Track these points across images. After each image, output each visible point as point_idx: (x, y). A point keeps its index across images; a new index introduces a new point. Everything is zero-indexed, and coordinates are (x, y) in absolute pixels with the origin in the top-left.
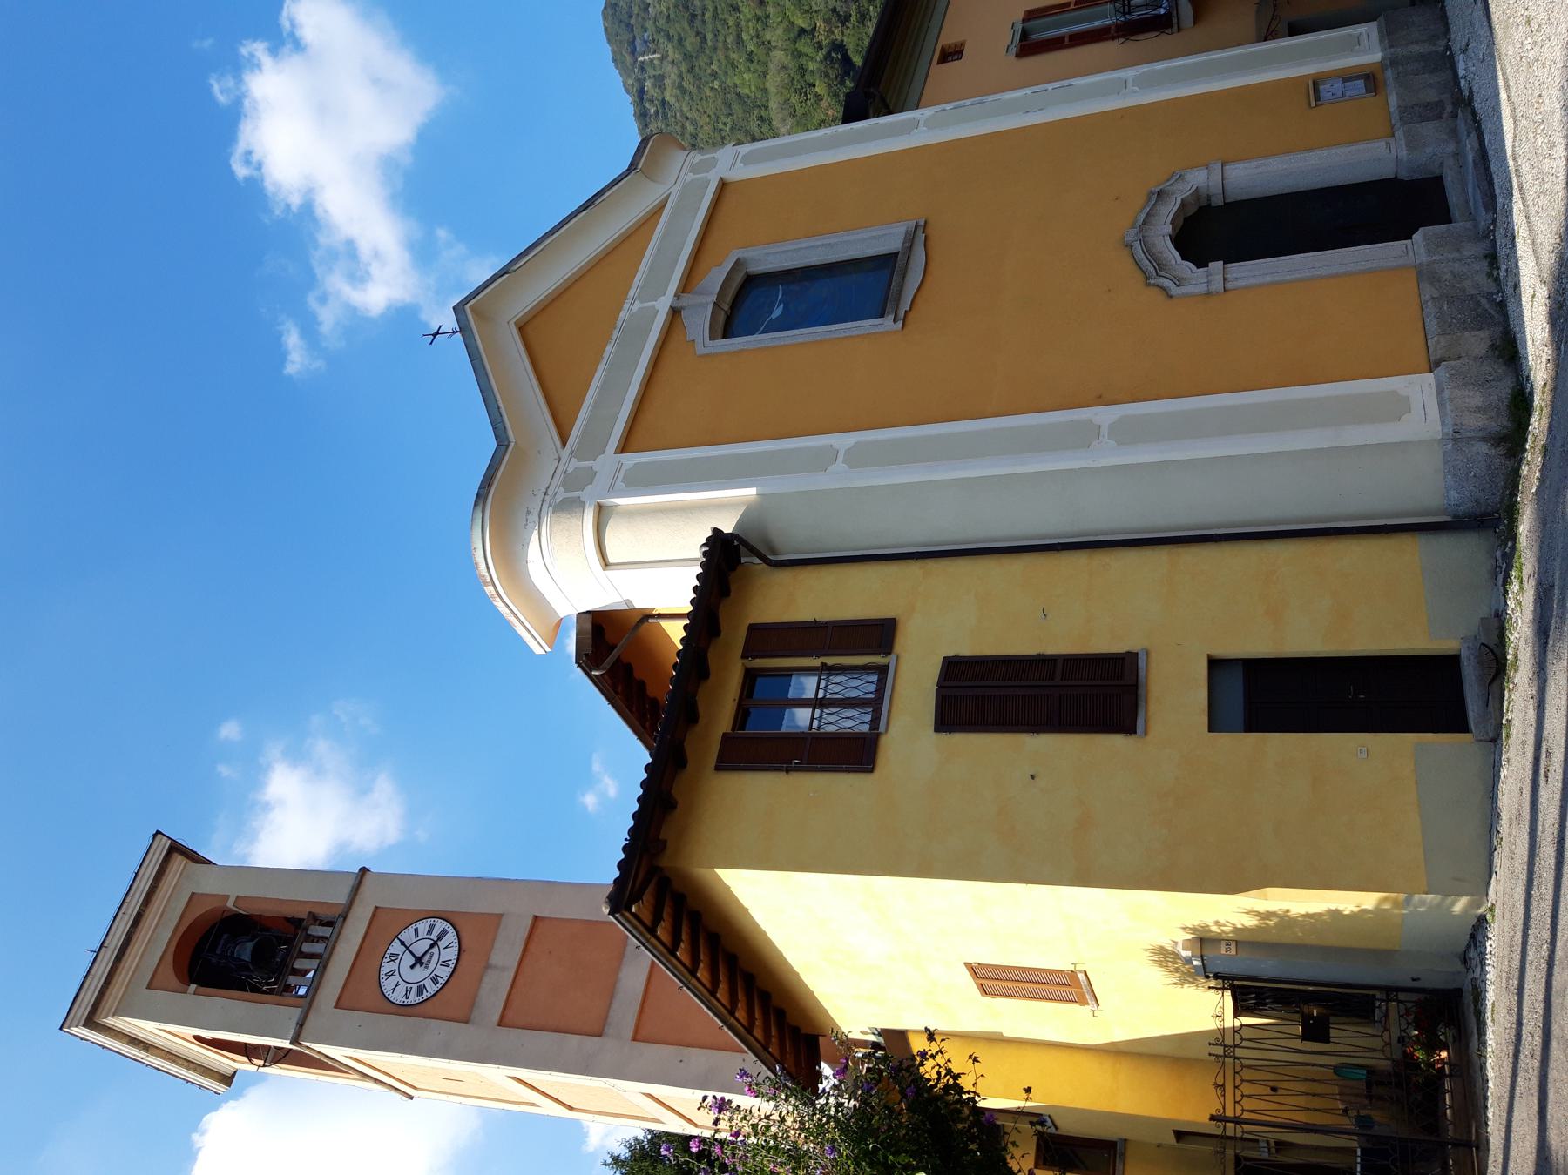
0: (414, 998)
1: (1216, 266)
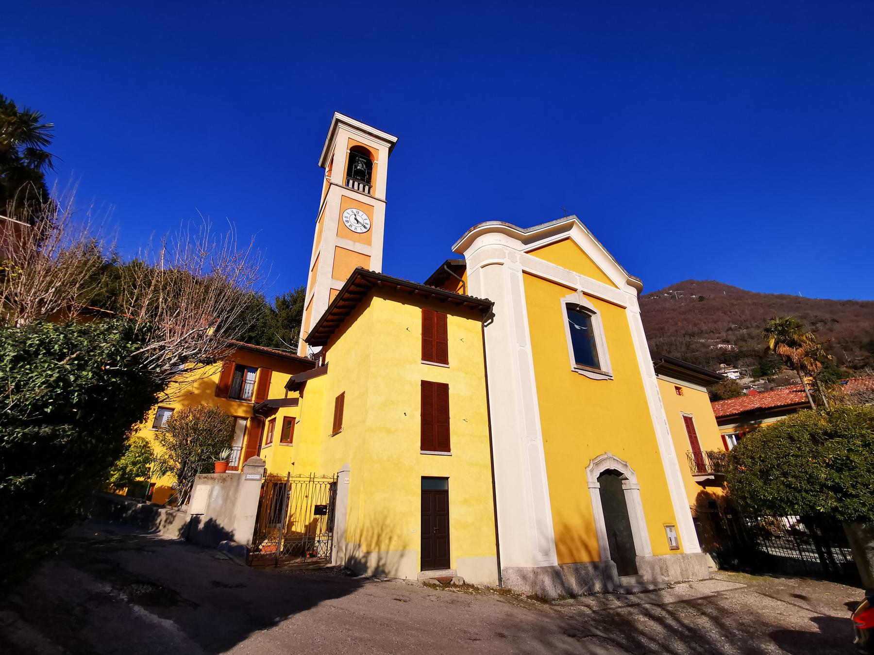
0: (345, 219)
1: (598, 485)
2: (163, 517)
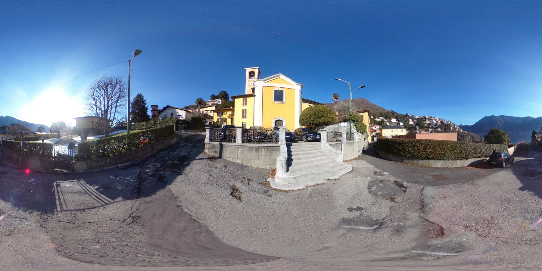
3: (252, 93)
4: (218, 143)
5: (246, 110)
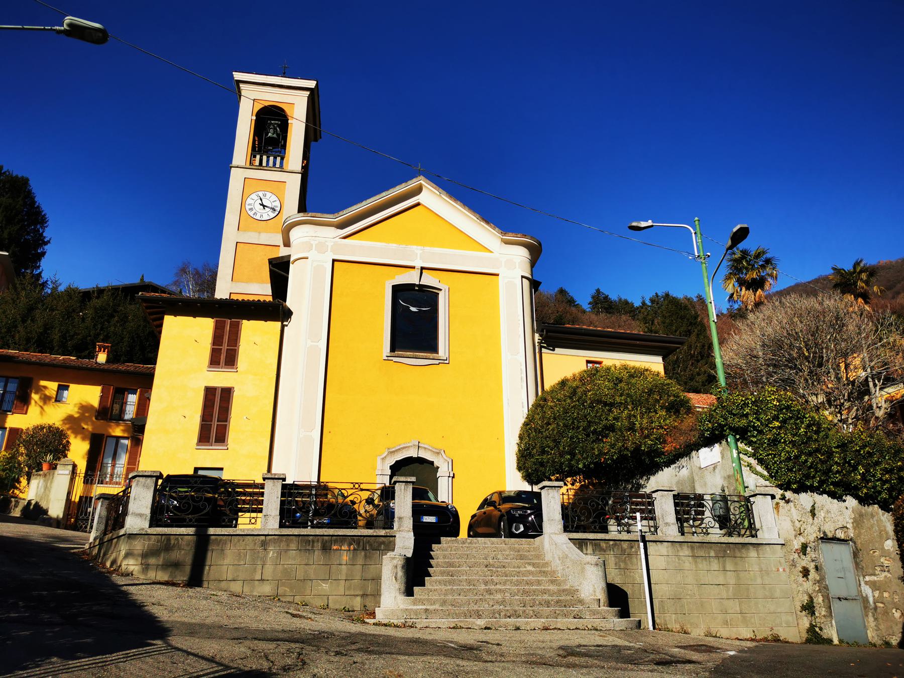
2: (13, 503)
3: (262, 290)
4: (191, 530)
5: (227, 393)
